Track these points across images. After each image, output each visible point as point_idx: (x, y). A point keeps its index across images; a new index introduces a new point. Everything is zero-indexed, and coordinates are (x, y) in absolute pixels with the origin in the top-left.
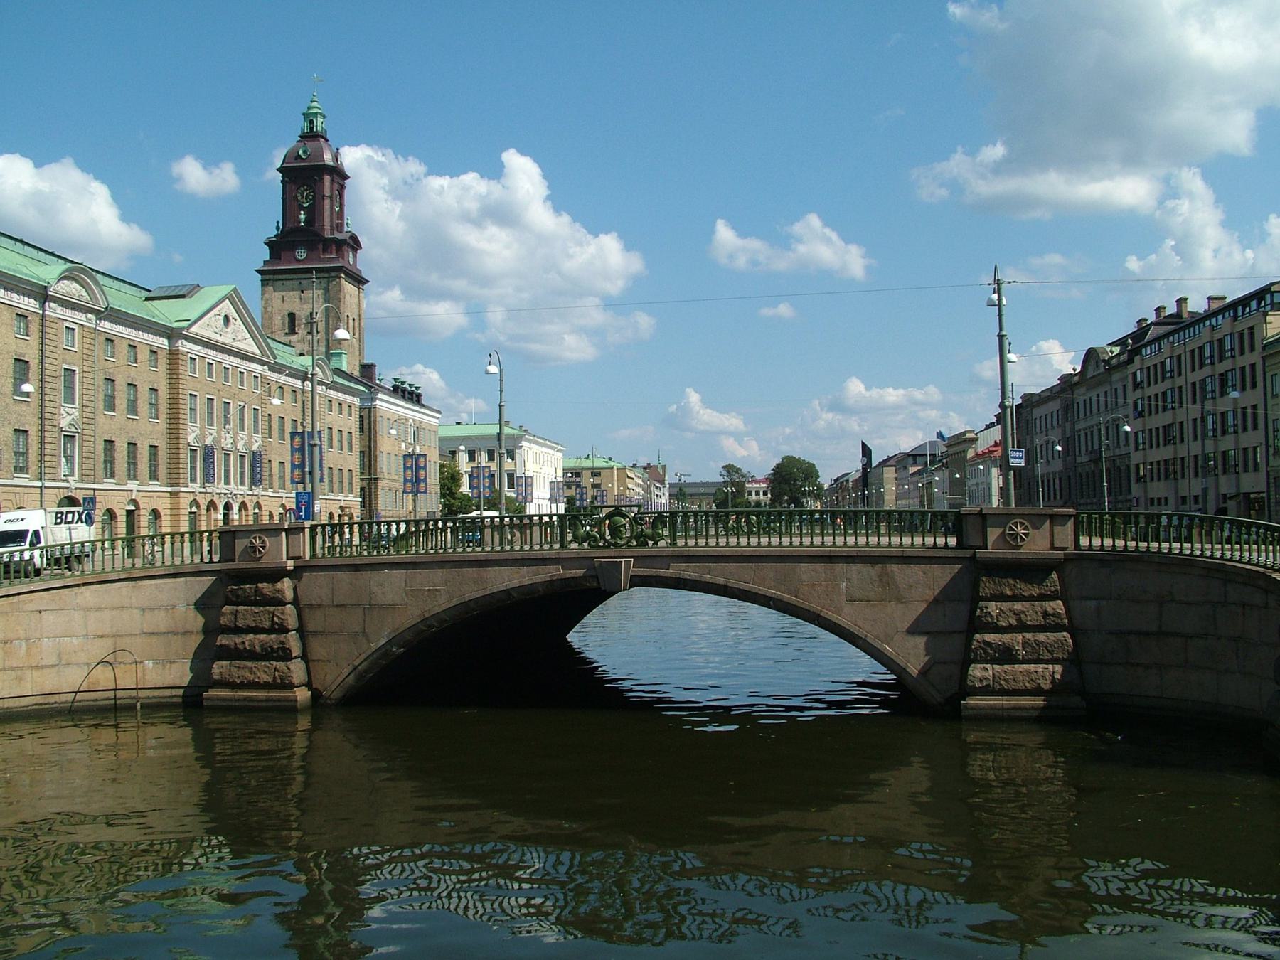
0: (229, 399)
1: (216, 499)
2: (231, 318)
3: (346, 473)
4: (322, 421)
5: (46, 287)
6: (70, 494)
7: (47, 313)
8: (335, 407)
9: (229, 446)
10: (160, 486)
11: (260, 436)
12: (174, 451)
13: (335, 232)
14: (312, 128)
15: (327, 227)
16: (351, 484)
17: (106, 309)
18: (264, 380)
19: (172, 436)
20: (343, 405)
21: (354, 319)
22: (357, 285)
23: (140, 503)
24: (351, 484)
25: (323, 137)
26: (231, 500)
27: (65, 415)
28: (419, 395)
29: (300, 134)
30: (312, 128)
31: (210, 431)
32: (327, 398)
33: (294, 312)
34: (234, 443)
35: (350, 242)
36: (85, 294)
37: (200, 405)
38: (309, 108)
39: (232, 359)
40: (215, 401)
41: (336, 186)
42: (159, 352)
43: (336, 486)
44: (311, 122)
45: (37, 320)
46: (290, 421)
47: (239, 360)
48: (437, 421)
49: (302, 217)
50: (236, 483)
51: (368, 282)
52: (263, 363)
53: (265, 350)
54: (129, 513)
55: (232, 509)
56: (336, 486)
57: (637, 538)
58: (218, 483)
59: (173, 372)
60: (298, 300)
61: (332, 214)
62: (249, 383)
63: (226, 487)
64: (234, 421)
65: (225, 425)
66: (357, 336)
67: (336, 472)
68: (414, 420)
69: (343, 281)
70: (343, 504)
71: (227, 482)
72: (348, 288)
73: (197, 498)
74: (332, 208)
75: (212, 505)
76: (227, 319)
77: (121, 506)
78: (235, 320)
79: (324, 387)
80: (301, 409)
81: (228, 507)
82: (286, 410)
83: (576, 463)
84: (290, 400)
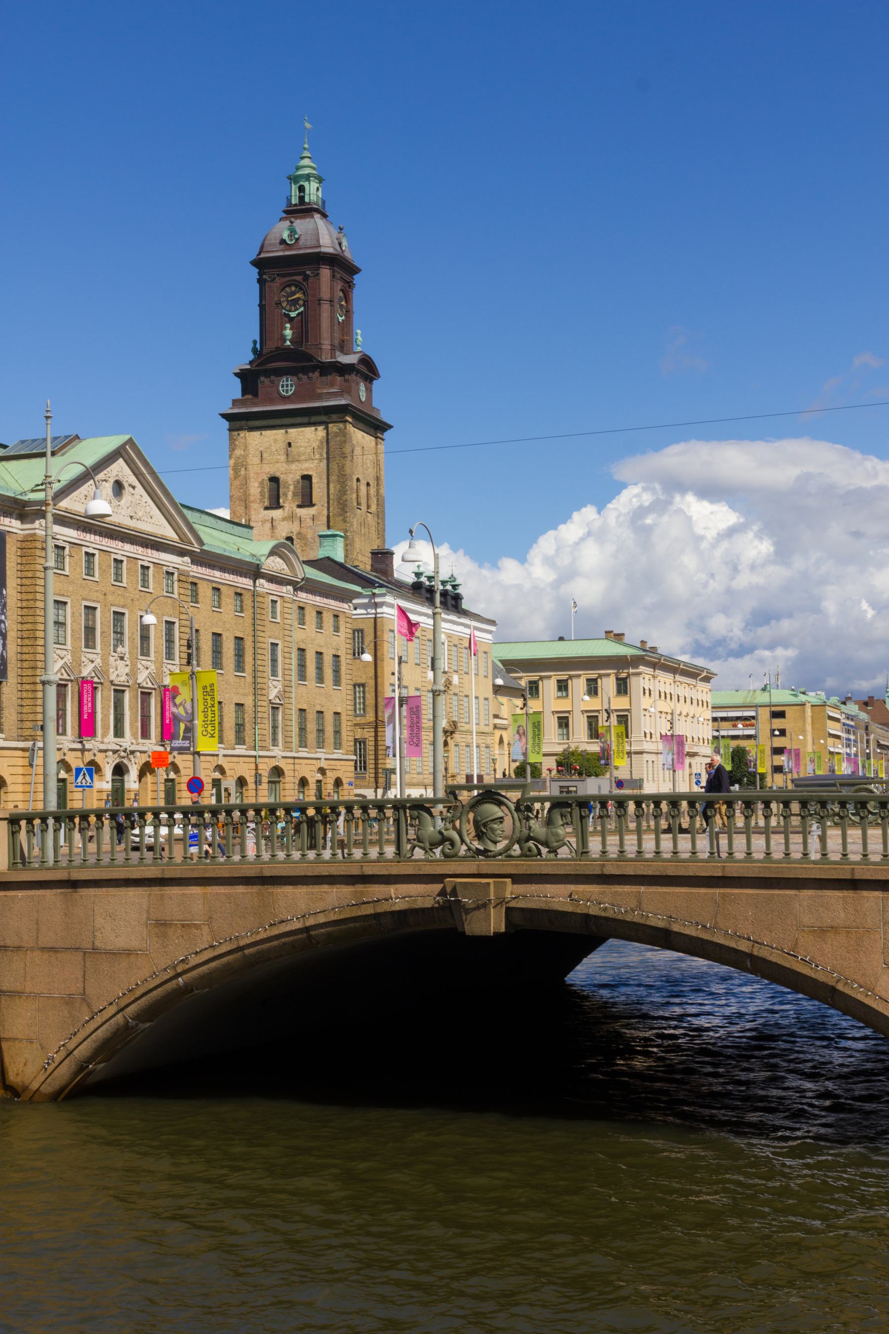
0: (123, 607)
1: (99, 759)
2: (126, 485)
3: (329, 718)
4: (287, 639)
5: (258, 565)
6: (277, 764)
7: (257, 589)
8: (311, 616)
9: (123, 678)
10: (5, 739)
11: (280, 678)
12: (28, 687)
13: (338, 353)
14: (302, 199)
15: (326, 345)
16: (337, 732)
17: (303, 579)
18: (183, 578)
19: (25, 664)
20: (325, 615)
21: (368, 484)
22: (372, 431)
23: (226, 769)
24: (337, 732)
25: (317, 211)
26: (125, 761)
27: (272, 687)
28: (457, 598)
29: (284, 207)
30: (302, 199)
31: (91, 656)
32: (298, 604)
33: (278, 474)
34: (133, 674)
35: (362, 368)
36: (285, 567)
37: (73, 617)
38: (298, 168)
39: (128, 547)
40: (127, 615)
41: (339, 285)
42: (222, 589)
43: (312, 737)
44: (302, 189)
45: (250, 594)
46: (232, 639)
47: (140, 549)
48: (489, 636)
49: (288, 333)
50: (134, 735)
51: (391, 427)
52: (182, 553)
53: (185, 534)
54: (319, 781)
55: (128, 771)
56: (312, 737)
57: (522, 841)
58: (104, 735)
59: (27, 568)
60: (283, 458)
61: (332, 326)
62: (103, 572)
63: (118, 740)
64: (132, 640)
65: (116, 646)
66: (373, 508)
67: (311, 716)
68: (449, 636)
69: (350, 428)
70: (323, 764)
71: (119, 732)
72: (360, 437)
73: (67, 758)
74: (333, 317)
75: (94, 768)
76: (119, 487)
77: (208, 772)
78: (134, 487)
79: (290, 588)
80: (250, 621)
81: (120, 770)
82: (224, 623)
83: (746, 697)
84: (232, 607)
